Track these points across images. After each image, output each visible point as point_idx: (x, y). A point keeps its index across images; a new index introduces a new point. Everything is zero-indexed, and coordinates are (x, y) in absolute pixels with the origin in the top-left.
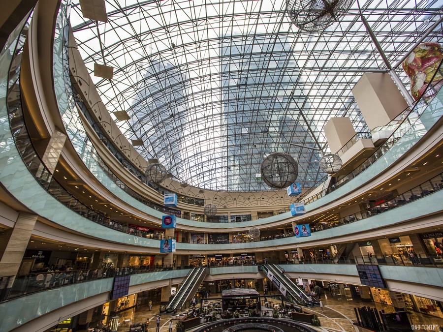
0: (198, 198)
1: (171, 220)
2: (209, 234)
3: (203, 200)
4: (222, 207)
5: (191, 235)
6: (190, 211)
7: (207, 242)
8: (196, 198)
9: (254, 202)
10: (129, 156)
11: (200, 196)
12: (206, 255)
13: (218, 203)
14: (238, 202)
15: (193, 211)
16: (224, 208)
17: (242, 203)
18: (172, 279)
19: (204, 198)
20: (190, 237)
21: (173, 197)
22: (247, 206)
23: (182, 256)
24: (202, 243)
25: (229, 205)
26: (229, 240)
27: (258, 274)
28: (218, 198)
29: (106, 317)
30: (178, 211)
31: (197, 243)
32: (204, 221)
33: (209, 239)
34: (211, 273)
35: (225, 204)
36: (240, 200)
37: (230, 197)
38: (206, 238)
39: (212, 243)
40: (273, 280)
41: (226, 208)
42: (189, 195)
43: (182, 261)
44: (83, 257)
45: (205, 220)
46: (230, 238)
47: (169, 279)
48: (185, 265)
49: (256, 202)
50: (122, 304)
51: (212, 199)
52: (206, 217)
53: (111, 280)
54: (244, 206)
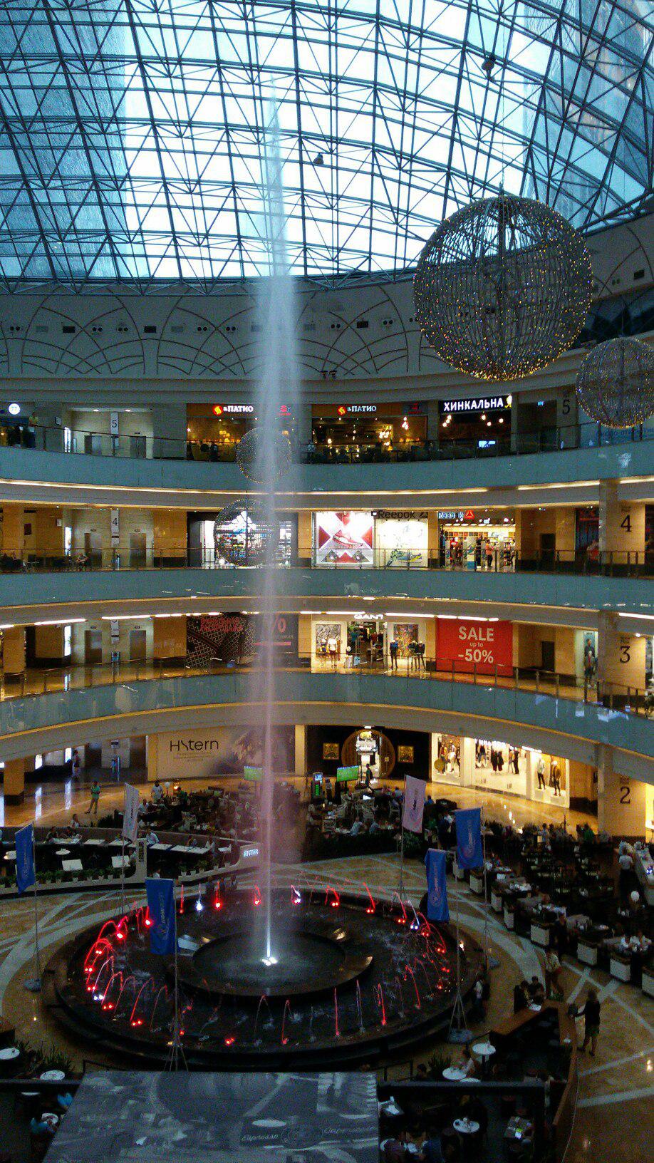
13: (191, 354)
14: (166, 349)
17: (55, 354)
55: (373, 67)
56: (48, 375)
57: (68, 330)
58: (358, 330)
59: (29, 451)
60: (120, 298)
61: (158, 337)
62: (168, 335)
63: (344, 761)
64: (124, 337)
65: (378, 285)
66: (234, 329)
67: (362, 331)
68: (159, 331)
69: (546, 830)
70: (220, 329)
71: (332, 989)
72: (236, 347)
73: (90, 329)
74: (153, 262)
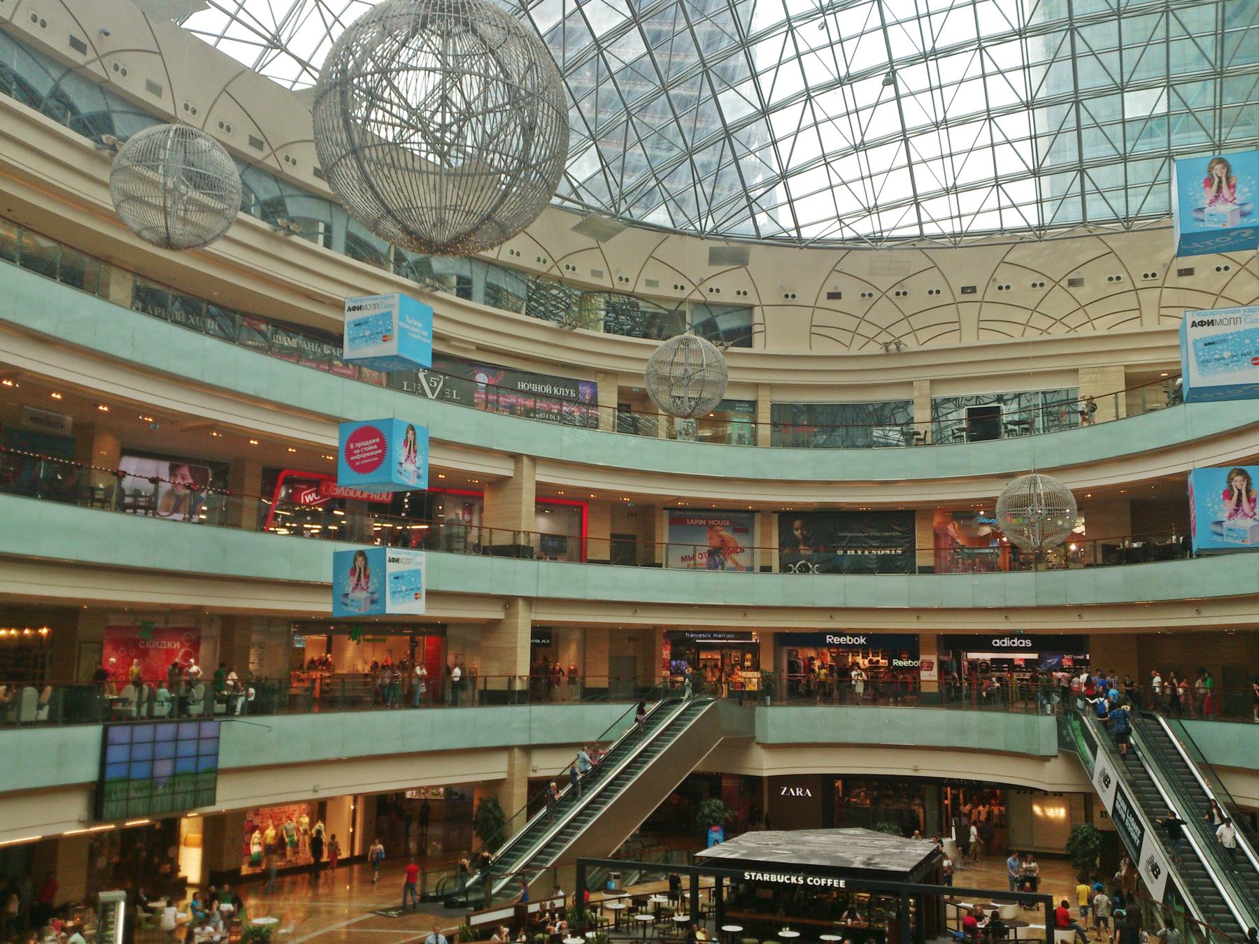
0: (712, 298)
1: (382, 445)
2: (787, 516)
3: (750, 308)
4: (874, 349)
5: (674, 522)
6: (756, 386)
7: (776, 565)
8: (696, 304)
9: (1114, 304)
10: (154, 88)
11: (728, 286)
12: (762, 632)
13: (851, 323)
14: (988, 312)
15: (772, 387)
16: (888, 355)
17: (1022, 316)
18: (528, 749)
19: (751, 299)
20: (663, 533)
21: (388, 316)
22: (1059, 332)
23: (614, 632)
24: (738, 568)
25: (923, 335)
26: (912, 551)
27: (1050, 766)
28: (851, 291)
29: (190, 893)
30: (574, 384)
31: (713, 566)
32: (754, 442)
33: (787, 542)
34: (759, 737)
35: (897, 331)
36: (1003, 296)
37: (932, 280)
38: (767, 540)
39: (805, 570)
40: (1115, 810)
41: (899, 354)
42: (650, 283)
43: (614, 659)
44: (35, 627)
45: (765, 431)
46: (923, 540)
47: (507, 749)
48: (640, 683)
49: (1129, 301)
50: (268, 850)
51: (805, 297)
52: (764, 414)
53: (90, 734)
54: (1032, 335)
55: (809, 192)
56: (842, 351)
57: (834, 296)
58: (1071, 290)
59: (755, 449)
60: (1101, 237)
61: (1129, 287)
62: (992, 294)
63: (466, 287)
64: (935, 300)
65: (1097, 235)
66: (905, 293)
67: (900, 301)
68: (980, 291)
69: (307, 838)
70: (1238, 267)
71: (242, 714)
72: (1220, 299)
73: (892, 293)
74: (966, 221)
